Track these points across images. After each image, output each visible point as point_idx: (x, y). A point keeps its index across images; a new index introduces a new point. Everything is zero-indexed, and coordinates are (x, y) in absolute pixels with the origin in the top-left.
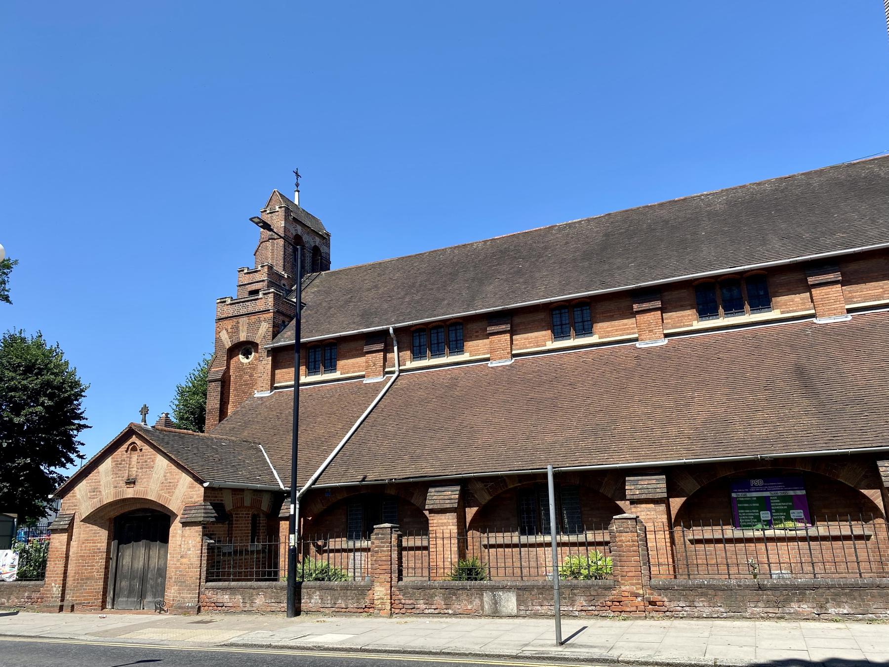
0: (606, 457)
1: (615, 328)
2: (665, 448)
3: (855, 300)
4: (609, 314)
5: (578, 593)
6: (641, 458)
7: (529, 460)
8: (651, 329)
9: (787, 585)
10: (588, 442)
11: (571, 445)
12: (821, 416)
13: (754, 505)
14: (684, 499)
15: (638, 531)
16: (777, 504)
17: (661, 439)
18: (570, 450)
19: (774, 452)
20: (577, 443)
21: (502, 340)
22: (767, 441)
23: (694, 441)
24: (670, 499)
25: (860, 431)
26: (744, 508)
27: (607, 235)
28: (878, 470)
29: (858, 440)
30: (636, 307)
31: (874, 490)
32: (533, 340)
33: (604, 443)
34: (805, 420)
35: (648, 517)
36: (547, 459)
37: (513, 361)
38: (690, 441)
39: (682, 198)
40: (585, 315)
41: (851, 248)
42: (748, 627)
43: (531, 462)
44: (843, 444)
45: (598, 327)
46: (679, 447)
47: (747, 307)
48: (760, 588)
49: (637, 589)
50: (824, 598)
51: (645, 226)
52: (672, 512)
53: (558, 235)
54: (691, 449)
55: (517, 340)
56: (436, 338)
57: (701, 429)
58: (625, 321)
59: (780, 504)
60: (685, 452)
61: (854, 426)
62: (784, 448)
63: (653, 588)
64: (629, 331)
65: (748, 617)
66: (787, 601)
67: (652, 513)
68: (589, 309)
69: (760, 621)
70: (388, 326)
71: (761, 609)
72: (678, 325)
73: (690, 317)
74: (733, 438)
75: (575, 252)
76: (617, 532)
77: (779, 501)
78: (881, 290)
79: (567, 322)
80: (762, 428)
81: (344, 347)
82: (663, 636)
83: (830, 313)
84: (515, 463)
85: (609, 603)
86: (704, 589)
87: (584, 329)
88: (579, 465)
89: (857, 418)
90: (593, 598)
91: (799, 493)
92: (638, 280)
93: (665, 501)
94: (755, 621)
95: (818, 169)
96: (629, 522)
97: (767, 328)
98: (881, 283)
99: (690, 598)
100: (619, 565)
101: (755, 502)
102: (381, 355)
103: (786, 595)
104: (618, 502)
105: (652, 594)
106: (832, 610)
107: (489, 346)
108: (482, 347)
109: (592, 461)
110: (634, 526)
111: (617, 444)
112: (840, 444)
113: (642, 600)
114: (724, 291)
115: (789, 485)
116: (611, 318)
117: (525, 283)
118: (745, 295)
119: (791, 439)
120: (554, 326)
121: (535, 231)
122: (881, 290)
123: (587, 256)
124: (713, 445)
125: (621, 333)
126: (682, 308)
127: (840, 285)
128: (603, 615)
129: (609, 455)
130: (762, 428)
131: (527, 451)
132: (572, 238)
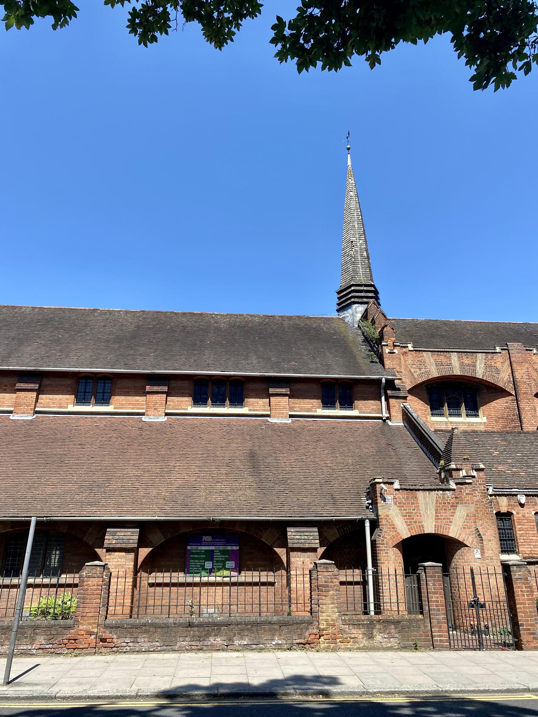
0: (95, 510)
1: (128, 402)
2: (144, 506)
3: (295, 409)
4: (126, 390)
5: (40, 632)
6: (123, 513)
7: (25, 508)
8: (156, 407)
9: (209, 622)
10: (83, 496)
11: (67, 498)
12: (258, 490)
13: (202, 556)
14: (151, 549)
15: (104, 577)
16: (218, 556)
17: (142, 498)
18: (65, 502)
19: (223, 515)
20: (73, 496)
21: (28, 397)
22: (219, 506)
23: (167, 502)
24: (140, 549)
25: (281, 505)
26: (194, 559)
27: (138, 327)
28: (287, 534)
29: (278, 510)
30: (148, 388)
31: (282, 549)
32: (57, 401)
33: (95, 498)
34: (249, 492)
35: (119, 563)
36: (42, 508)
37: (34, 417)
38: (164, 502)
39: (199, 313)
40: (106, 388)
41: (298, 373)
42: (174, 659)
43: (26, 510)
44: (269, 513)
45: (115, 399)
46: (155, 506)
47: (228, 402)
48: (189, 625)
49: (93, 628)
50: (233, 633)
51: (168, 327)
52: (139, 560)
53: (99, 318)
54: (164, 509)
55: (42, 399)
56: (102, 388)
57: (175, 492)
58: (138, 398)
59: (220, 556)
60: (158, 510)
61: (278, 500)
62: (230, 513)
63: (106, 627)
64: (139, 407)
65: (176, 649)
66: (208, 635)
67: (123, 560)
68: (111, 383)
69: (185, 653)
70: (381, 377)
71: (187, 643)
72: (177, 407)
73: (187, 403)
74: (196, 502)
75: (110, 334)
76: (86, 577)
77: (219, 554)
78: (311, 405)
79: (90, 391)
80: (218, 496)
81: (359, 388)
82: (103, 670)
83: (281, 416)
84: (11, 510)
85: (66, 641)
86: (147, 627)
87: (103, 399)
88: (70, 515)
89: (281, 494)
90: (52, 636)
91: (235, 548)
92: (154, 367)
93: (135, 551)
94: (180, 653)
95: (289, 315)
96: (98, 568)
97: (238, 420)
98: (312, 401)
99: (135, 634)
100: (82, 607)
101: (203, 554)
102: (34, 395)
103: (207, 631)
104: (96, 550)
105: (104, 632)
106: (236, 642)
107: (14, 400)
108: (8, 400)
109: (82, 513)
110: (102, 572)
111: (107, 500)
112: (266, 513)
113: (95, 638)
114: (214, 388)
115: (229, 542)
116: (127, 393)
117: (61, 351)
118: (228, 393)
119: (236, 506)
120: (78, 392)
121: (80, 309)
122: (311, 405)
123: (118, 340)
124: (181, 506)
125: (132, 407)
126: (182, 395)
127: (288, 398)
128: (58, 652)
129: (97, 508)
130: (218, 496)
131: (26, 500)
132: (110, 322)
